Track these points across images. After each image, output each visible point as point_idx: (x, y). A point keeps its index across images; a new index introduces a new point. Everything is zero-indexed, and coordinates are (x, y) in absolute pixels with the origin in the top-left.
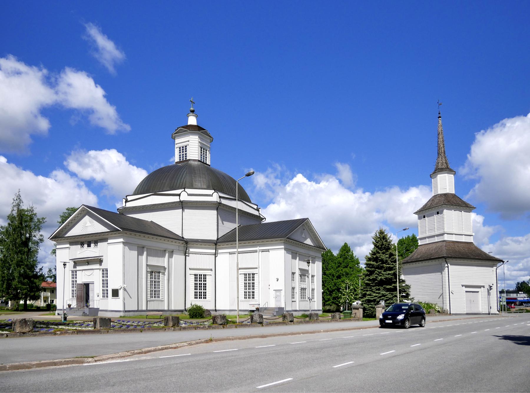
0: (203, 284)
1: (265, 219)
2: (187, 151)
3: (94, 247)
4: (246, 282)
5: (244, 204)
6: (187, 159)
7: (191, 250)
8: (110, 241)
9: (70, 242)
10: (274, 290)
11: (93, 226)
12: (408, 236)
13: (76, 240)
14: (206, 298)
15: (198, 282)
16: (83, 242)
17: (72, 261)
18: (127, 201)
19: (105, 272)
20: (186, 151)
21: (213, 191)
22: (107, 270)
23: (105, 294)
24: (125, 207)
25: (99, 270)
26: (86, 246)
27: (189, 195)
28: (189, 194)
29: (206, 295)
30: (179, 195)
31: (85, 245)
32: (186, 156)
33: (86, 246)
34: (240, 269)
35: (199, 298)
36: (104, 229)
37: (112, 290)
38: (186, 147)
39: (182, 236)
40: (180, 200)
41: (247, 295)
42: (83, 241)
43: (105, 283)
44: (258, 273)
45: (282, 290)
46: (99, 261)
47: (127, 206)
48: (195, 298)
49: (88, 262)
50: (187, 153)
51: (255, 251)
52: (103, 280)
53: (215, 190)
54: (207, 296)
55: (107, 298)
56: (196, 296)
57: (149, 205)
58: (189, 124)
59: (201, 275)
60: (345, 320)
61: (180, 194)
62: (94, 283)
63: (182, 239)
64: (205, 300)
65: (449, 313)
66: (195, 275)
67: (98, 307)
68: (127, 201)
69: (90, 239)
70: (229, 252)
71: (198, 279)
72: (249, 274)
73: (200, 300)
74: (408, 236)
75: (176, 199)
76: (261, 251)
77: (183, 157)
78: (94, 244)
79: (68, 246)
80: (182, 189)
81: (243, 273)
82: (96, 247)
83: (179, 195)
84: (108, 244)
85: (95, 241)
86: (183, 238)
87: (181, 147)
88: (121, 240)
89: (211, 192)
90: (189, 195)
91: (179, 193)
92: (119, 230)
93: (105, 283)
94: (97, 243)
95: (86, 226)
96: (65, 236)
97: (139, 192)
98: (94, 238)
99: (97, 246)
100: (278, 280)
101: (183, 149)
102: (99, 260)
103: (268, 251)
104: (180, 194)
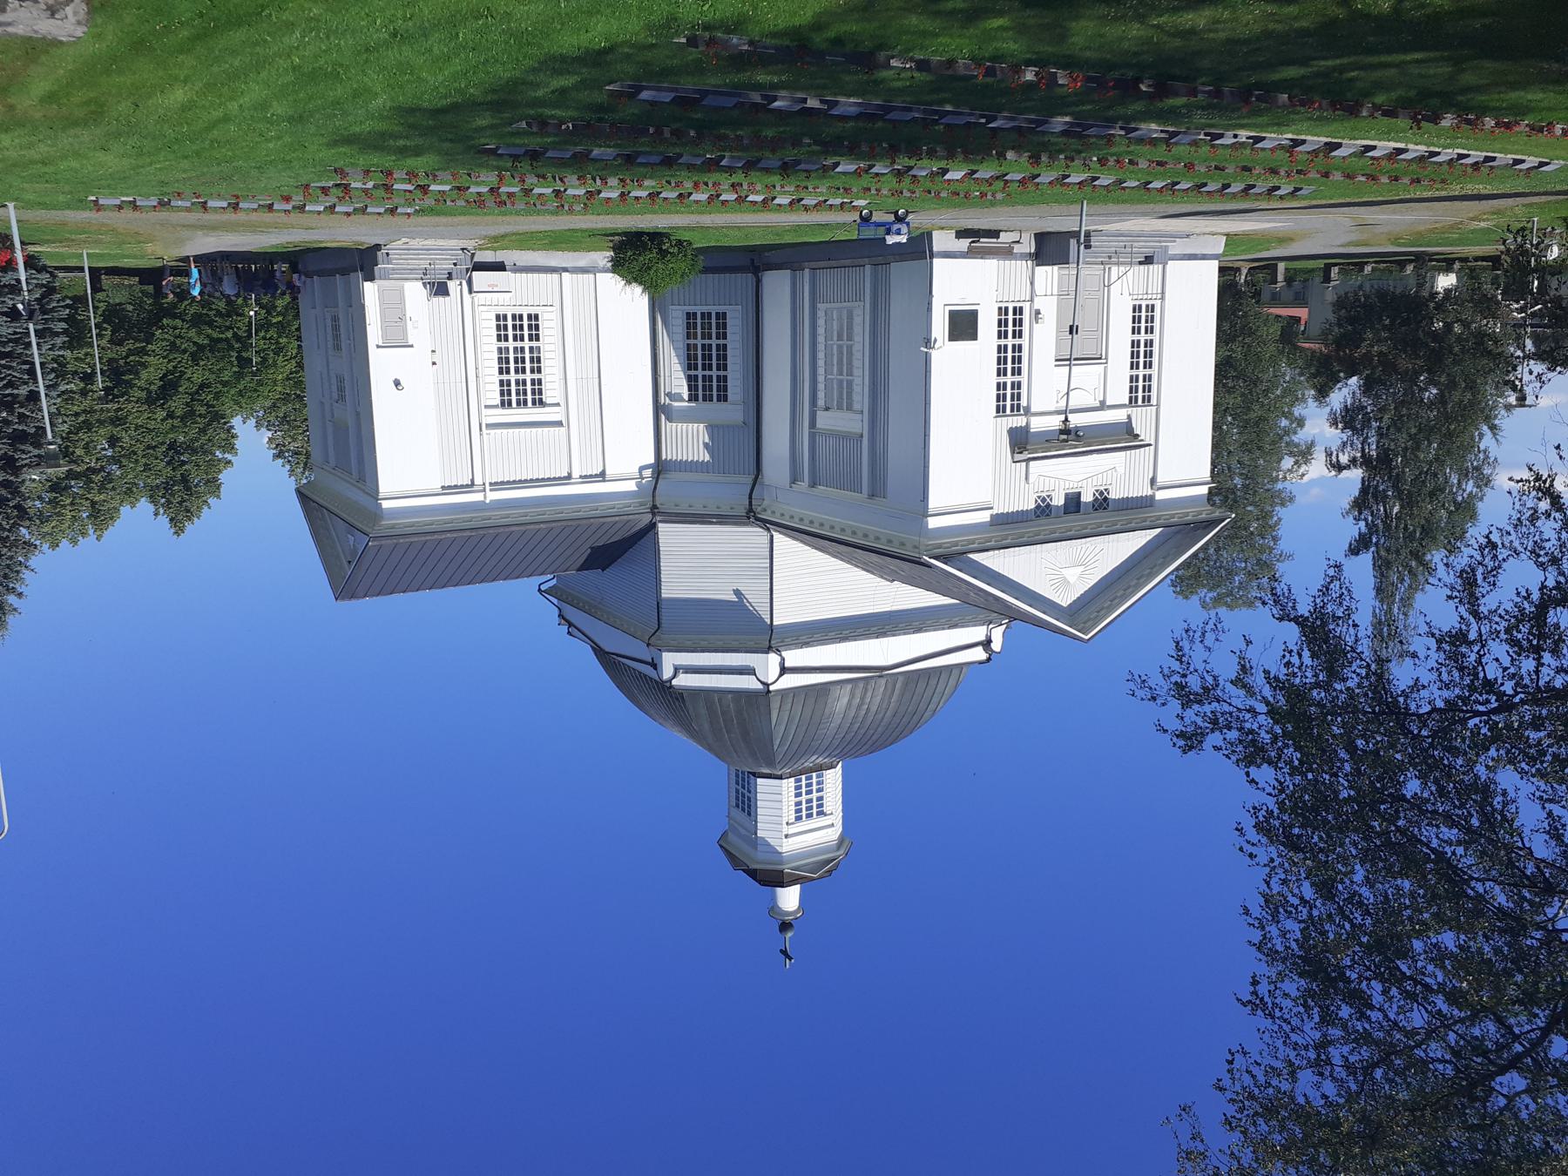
0: (528, 370)
1: (539, 590)
2: (793, 803)
3: (1053, 494)
4: (505, 377)
5: (598, 642)
6: (792, 779)
7: (631, 486)
8: (984, 517)
9: (1151, 506)
10: (412, 346)
11: (1054, 567)
12: (74, 542)
13: (1122, 518)
14: (498, 317)
15: (513, 377)
16: (1038, 516)
17: (1142, 440)
18: (986, 644)
19: (1009, 399)
20: (798, 804)
21: (674, 682)
22: (998, 411)
23: (1012, 321)
24: (991, 626)
25: (1108, 403)
26: (1087, 497)
27: (749, 671)
28: (749, 674)
29: (498, 328)
30: (784, 670)
31: (1062, 502)
32: (798, 788)
33: (1087, 497)
34: (559, 424)
35: (521, 317)
36: (992, 560)
37: (975, 338)
38: (799, 819)
39: (772, 536)
40: (780, 655)
41: (526, 327)
42: (1097, 514)
43: (1010, 361)
44: (563, 403)
45: (378, 347)
46: (1021, 442)
47: (985, 627)
48: (536, 317)
49: (1069, 439)
50: (793, 798)
51: (497, 486)
52: (1147, 365)
53: (671, 687)
54: (494, 323)
55: (1003, 305)
56: (502, 323)
57: (899, 635)
58: (798, 886)
59: (518, 403)
60: (528, 213)
61: (781, 675)
62: (1057, 360)
63: (765, 524)
64: (691, 309)
65: (1085, 202)
66: (542, 403)
67: (435, 299)
68: (986, 644)
69: (1073, 521)
70: (659, 410)
71: (513, 388)
72: (522, 403)
73: (705, 309)
74: (74, 542)
75: (794, 657)
76: (475, 488)
77: (810, 785)
78: (1054, 503)
79: (1161, 495)
80: (777, 691)
81: (547, 409)
82: (1044, 495)
83: (784, 670)
84: (992, 508)
85: (1105, 508)
86: (768, 529)
87: (815, 816)
88: (933, 523)
89: (683, 681)
90: (749, 671)
91: (785, 676)
92: (936, 558)
93: (1010, 361)
94: (1038, 507)
95: (1082, 568)
96: (1160, 529)
97: (956, 672)
98: (1044, 526)
99: (1039, 497)
100: (397, 383)
101: (809, 809)
102: (1028, 447)
103: (448, 489)
104: (781, 675)
